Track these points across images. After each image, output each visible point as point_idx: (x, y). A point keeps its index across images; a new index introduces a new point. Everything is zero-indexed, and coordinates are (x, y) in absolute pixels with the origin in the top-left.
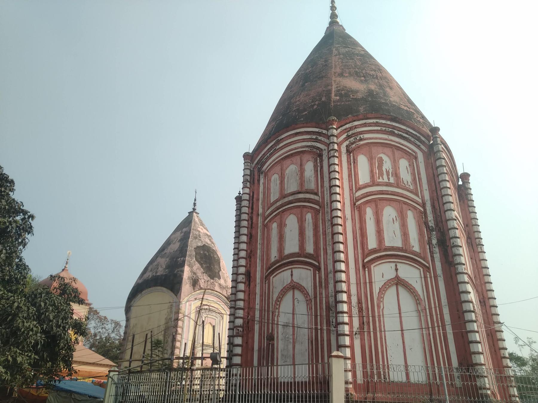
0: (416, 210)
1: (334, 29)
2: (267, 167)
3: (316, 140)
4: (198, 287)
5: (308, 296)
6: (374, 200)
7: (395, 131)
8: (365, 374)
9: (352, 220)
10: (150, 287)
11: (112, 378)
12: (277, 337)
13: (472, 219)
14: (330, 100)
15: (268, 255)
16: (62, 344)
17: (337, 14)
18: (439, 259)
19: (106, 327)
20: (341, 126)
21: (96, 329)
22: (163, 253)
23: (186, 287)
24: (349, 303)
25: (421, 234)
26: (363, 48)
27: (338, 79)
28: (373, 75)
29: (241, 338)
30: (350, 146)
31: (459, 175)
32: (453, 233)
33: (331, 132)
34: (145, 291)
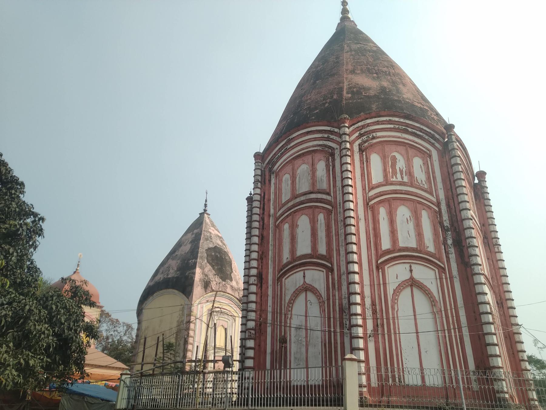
2: (279, 167)
3: (328, 139)
4: (210, 289)
5: (321, 299)
6: (388, 200)
7: (408, 129)
8: (380, 377)
9: (365, 220)
10: (162, 290)
11: (124, 382)
12: (290, 340)
14: (342, 98)
16: (74, 347)
17: (349, 9)
20: (353, 125)
22: (174, 255)
23: (198, 289)
24: (363, 305)
25: (436, 234)
26: (375, 44)
27: (350, 76)
28: (386, 72)
30: (362, 144)
31: (475, 173)
32: (469, 233)
33: (343, 130)
34: (156, 293)
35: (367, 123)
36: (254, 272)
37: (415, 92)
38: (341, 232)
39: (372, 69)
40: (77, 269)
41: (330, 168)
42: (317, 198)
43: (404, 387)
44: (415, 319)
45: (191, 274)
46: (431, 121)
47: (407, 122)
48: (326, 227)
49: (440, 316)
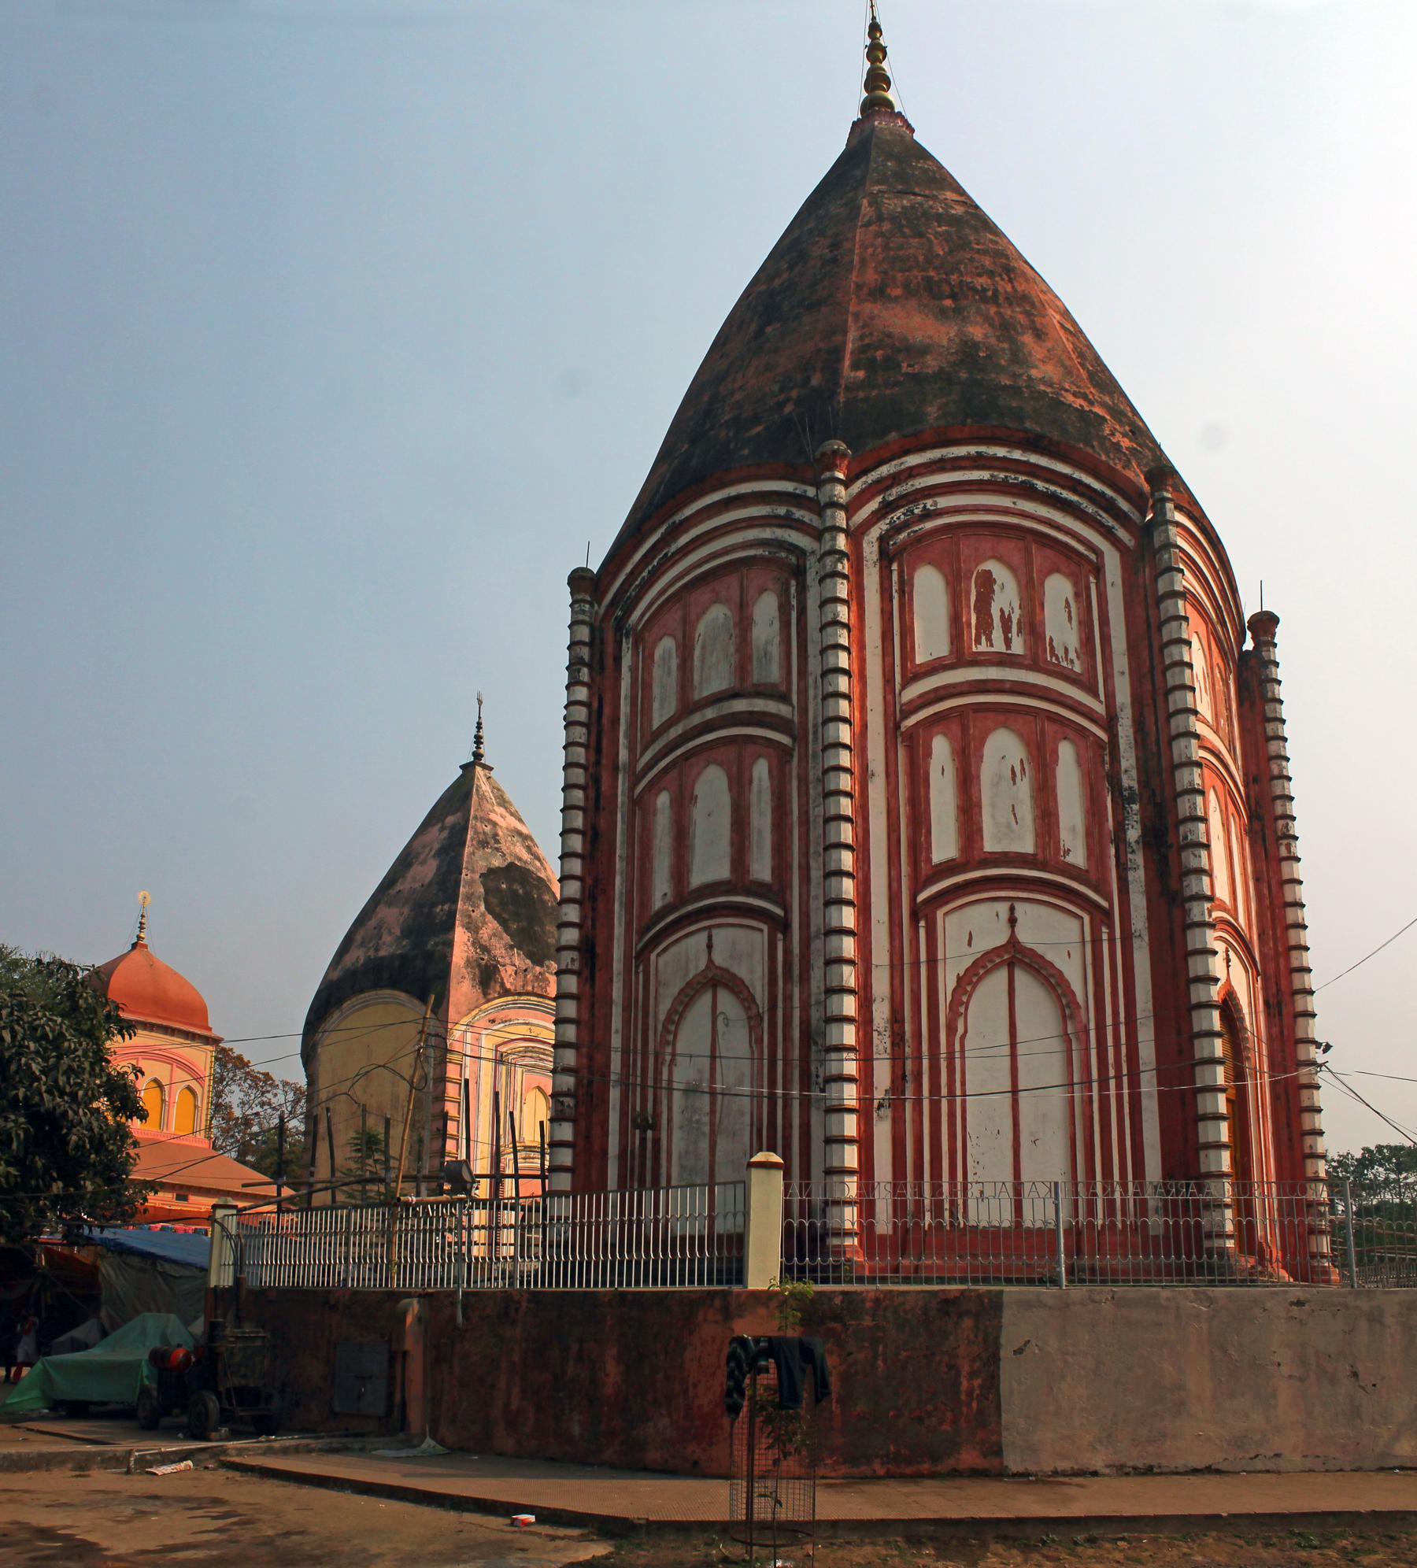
1: (873, 128)
2: (643, 615)
3: (788, 522)
4: (498, 988)
5: (754, 1006)
7: (1035, 482)
8: (899, 1208)
10: (362, 991)
12: (670, 1120)
14: (837, 384)
17: (889, 74)
18: (1143, 885)
19: (272, 1101)
21: (247, 1106)
22: (392, 892)
23: (462, 989)
25: (1094, 812)
27: (868, 308)
28: (984, 290)
29: (571, 1124)
31: (1247, 618)
32: (1188, 805)
34: (349, 1002)
35: (907, 465)
37: (1070, 358)
38: (816, 813)
39: (941, 280)
40: (139, 937)
41: (790, 614)
44: (1013, 1056)
45: (440, 948)
46: (1107, 454)
47: (1034, 459)
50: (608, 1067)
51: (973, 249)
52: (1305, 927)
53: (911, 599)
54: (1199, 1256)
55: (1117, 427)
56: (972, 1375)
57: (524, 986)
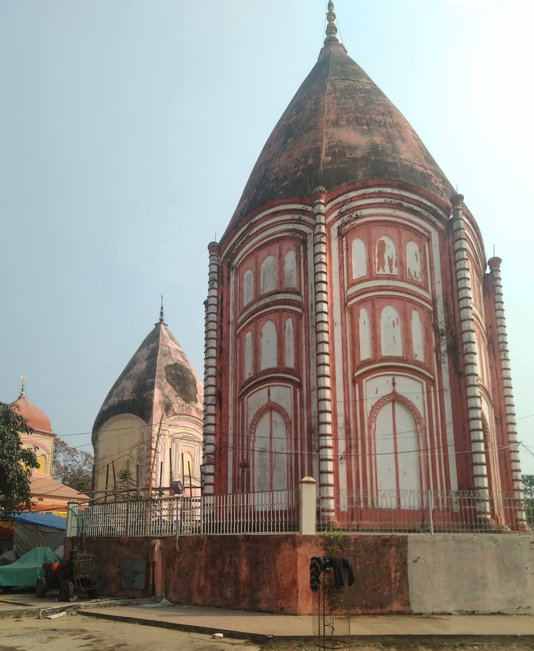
0: (424, 309)
1: (330, 51)
2: (239, 261)
3: (299, 221)
4: (172, 412)
5: (288, 418)
6: (371, 299)
8: (350, 500)
9: (342, 325)
10: (117, 414)
11: (72, 511)
12: (253, 464)
13: (497, 318)
14: (320, 163)
15: (242, 371)
16: (11, 476)
17: (337, 26)
20: (332, 200)
22: (128, 374)
23: (157, 413)
24: (335, 424)
25: (427, 339)
26: (370, 79)
27: (332, 130)
28: (380, 121)
30: (342, 227)
31: (487, 260)
32: (467, 337)
33: (318, 209)
36: (212, 390)
39: (362, 118)
40: (21, 394)
41: (301, 260)
42: (285, 299)
43: (376, 510)
44: (395, 438)
45: (149, 396)
47: (403, 193)
48: (294, 335)
49: (424, 435)
50: (227, 443)
51: (375, 103)
52: (512, 388)
53: (351, 253)
54: (476, 523)
55: (437, 179)
56: (396, 571)
57: (182, 412)
